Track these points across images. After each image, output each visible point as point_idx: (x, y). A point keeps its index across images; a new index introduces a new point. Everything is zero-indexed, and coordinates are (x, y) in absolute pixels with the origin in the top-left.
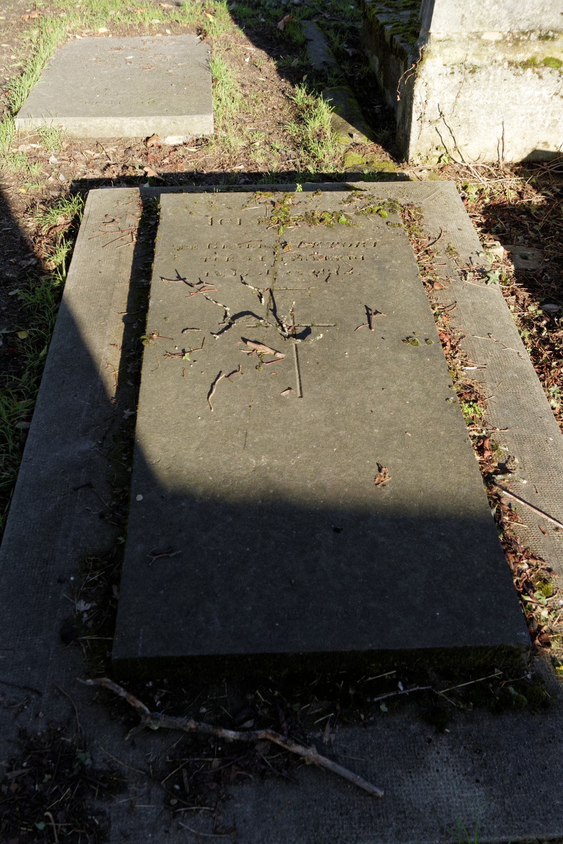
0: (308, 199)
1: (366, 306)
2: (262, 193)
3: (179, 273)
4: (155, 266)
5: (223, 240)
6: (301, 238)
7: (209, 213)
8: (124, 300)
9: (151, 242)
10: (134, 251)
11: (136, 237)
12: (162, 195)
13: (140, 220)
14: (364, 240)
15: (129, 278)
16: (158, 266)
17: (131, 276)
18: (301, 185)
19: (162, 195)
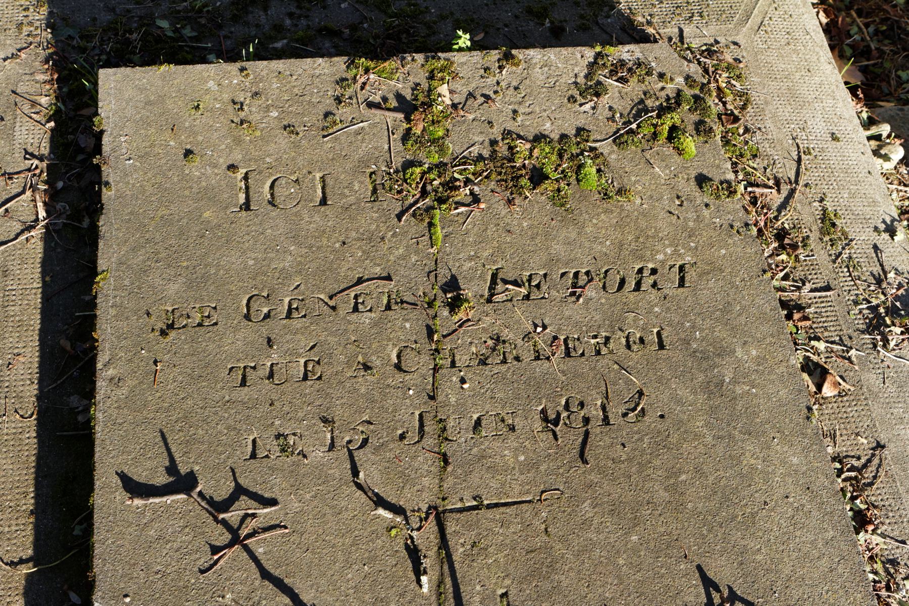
0: (491, 80)
1: (699, 568)
2: (371, 64)
3: (177, 456)
4: (100, 416)
5: (285, 275)
6: (492, 259)
7: (237, 157)
8: (26, 494)
9: (86, 223)
10: (45, 263)
11: (45, 203)
12: (103, 73)
13: (52, 130)
14: (653, 259)
15: (34, 389)
16: (110, 291)
17: (41, 381)
18: (468, 36)
19: (103, 73)
